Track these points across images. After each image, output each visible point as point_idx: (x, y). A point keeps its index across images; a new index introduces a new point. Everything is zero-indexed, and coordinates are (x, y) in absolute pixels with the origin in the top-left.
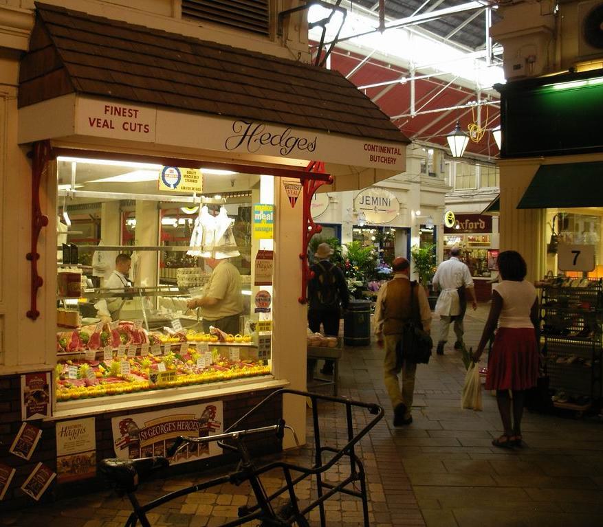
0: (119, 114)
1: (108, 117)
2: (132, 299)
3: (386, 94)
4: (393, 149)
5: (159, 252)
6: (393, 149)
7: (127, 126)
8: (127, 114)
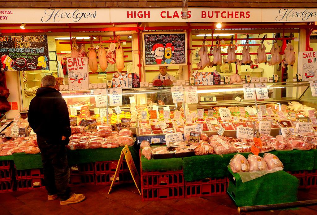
2: (275, 137)
4: (6, 11)
5: (274, 40)
6: (6, 11)
8: (245, 15)
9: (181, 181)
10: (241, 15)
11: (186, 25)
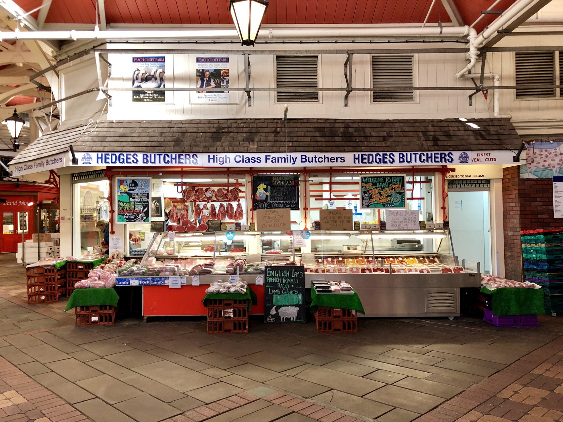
0: (483, 156)
1: (479, 157)
3: (432, 10)
7: (487, 160)
8: (486, 155)
9: (245, 315)
10: (441, 157)
11: (303, 169)
